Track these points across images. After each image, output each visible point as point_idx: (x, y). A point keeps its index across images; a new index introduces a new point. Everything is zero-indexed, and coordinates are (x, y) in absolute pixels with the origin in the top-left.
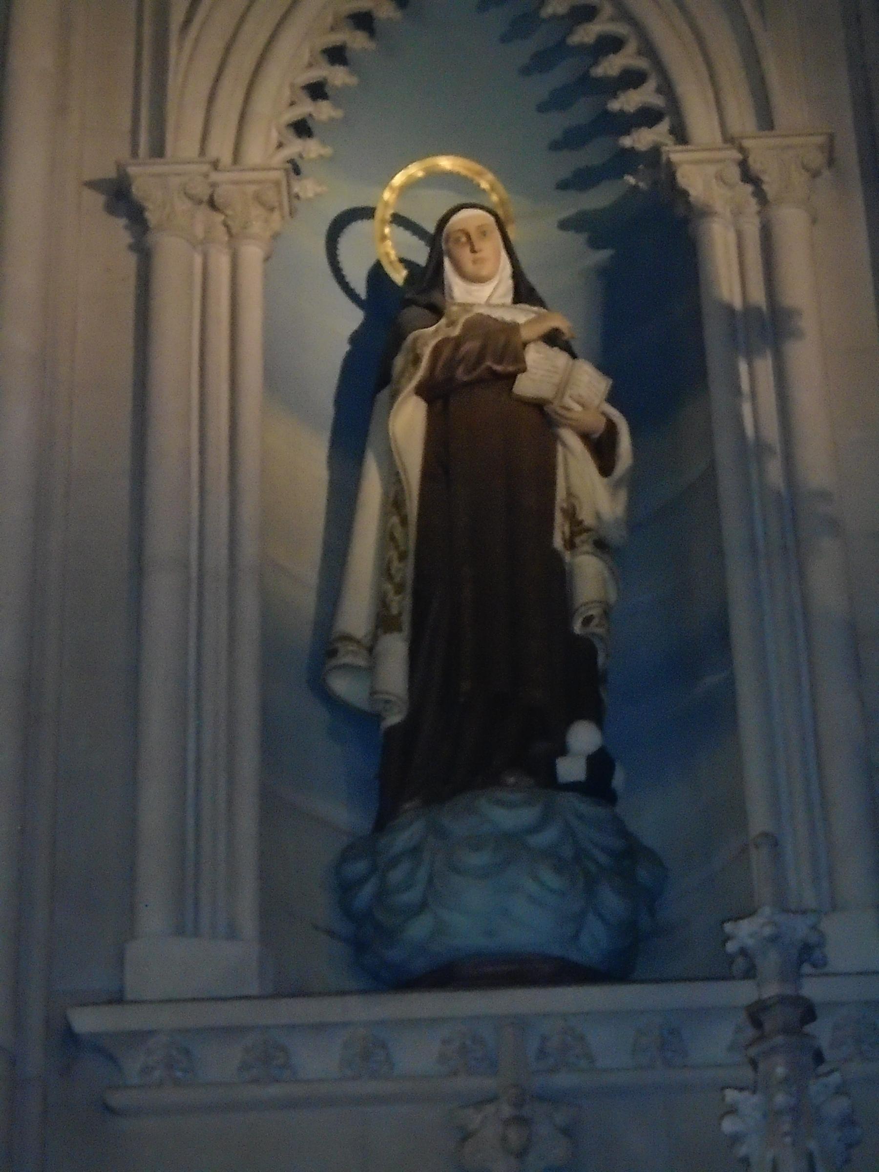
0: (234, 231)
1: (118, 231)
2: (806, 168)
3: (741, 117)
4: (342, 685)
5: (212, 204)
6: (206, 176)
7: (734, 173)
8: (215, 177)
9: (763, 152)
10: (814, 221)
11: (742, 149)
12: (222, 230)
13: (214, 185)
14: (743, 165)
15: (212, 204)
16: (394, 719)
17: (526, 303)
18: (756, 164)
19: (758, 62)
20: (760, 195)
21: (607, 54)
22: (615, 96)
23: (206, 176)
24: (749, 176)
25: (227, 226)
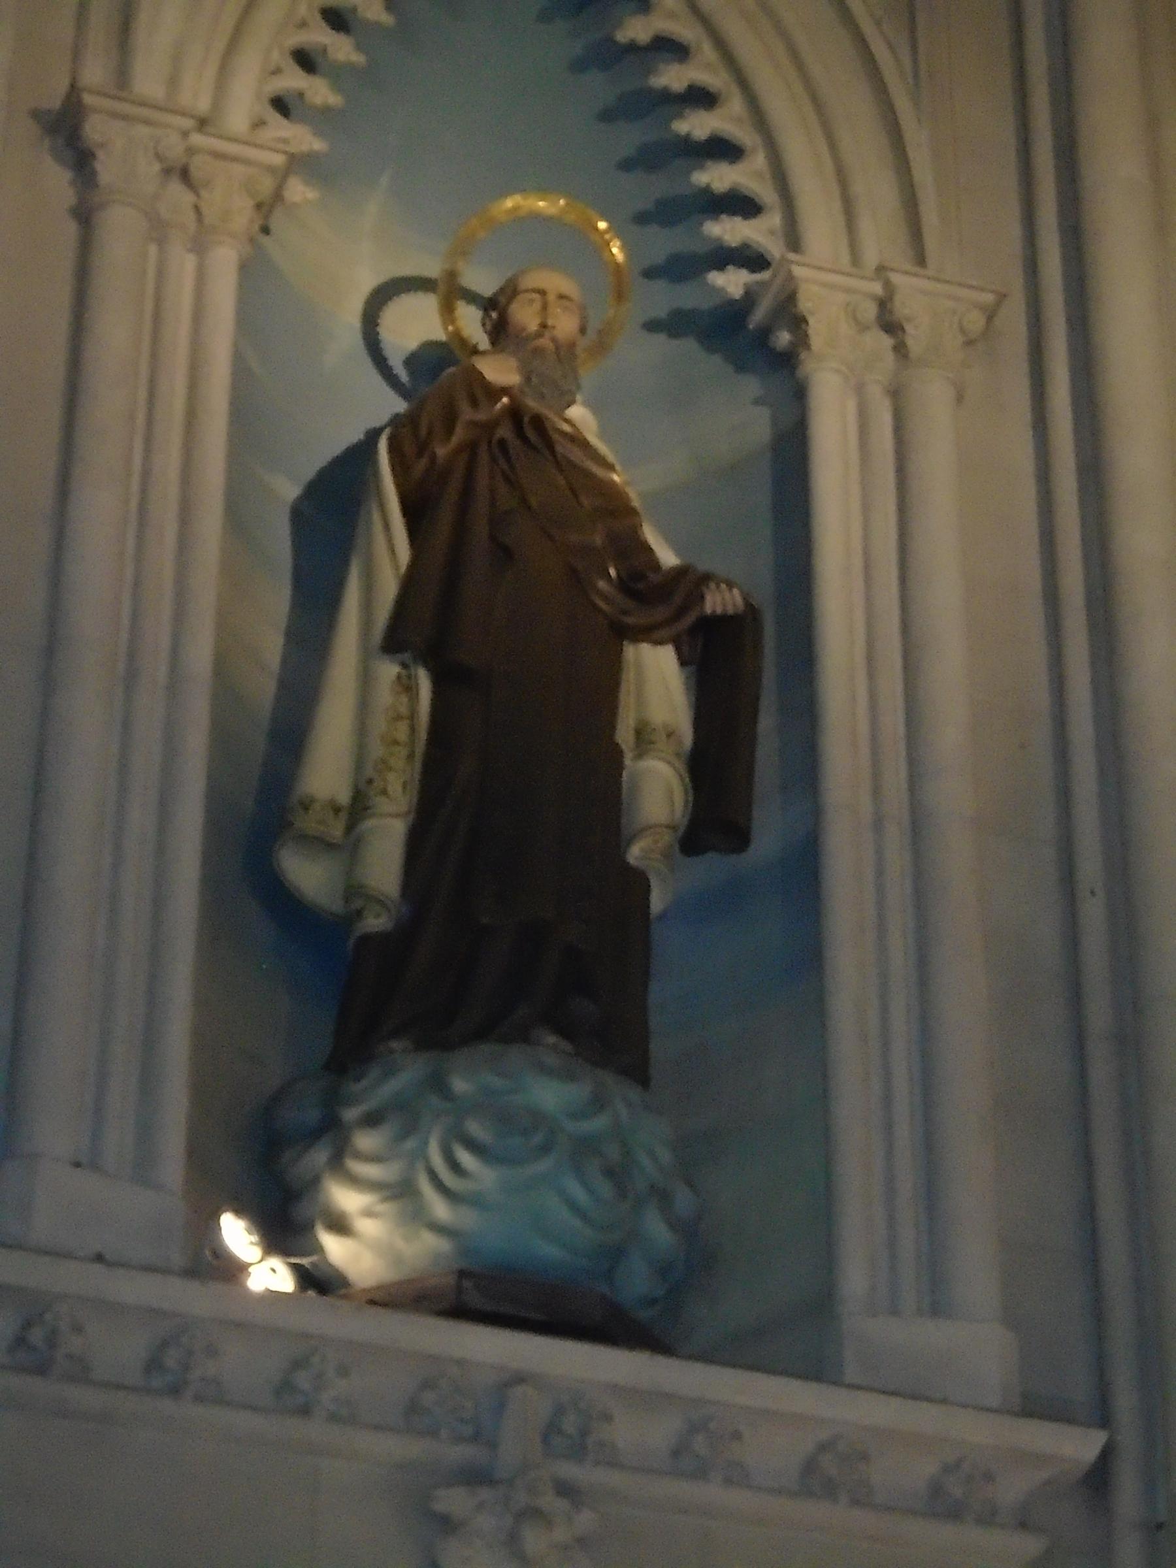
0: (207, 221)
1: (58, 180)
2: (962, 330)
3: (880, 235)
4: (309, 875)
5: (185, 175)
6: (185, 134)
7: (870, 311)
8: (197, 139)
9: (915, 297)
10: (960, 398)
11: (887, 285)
12: (191, 216)
13: (191, 151)
14: (884, 304)
15: (185, 175)
16: (376, 922)
17: (434, 692)
18: (903, 307)
19: (908, 170)
20: (900, 349)
21: (734, 213)
22: (680, 116)
23: (185, 134)
24: (891, 326)
25: (197, 209)
